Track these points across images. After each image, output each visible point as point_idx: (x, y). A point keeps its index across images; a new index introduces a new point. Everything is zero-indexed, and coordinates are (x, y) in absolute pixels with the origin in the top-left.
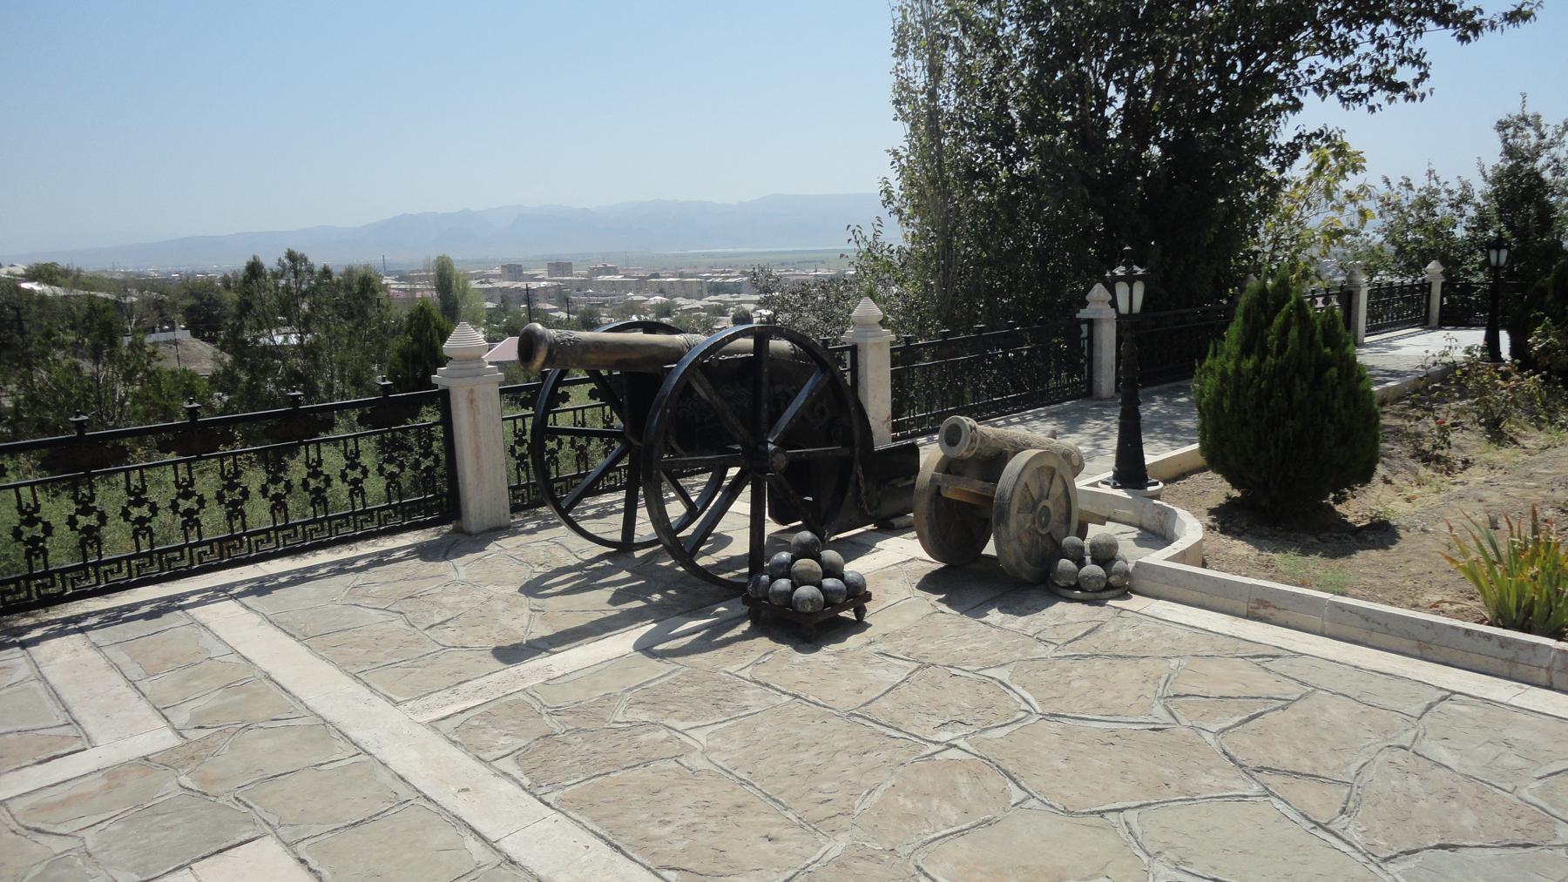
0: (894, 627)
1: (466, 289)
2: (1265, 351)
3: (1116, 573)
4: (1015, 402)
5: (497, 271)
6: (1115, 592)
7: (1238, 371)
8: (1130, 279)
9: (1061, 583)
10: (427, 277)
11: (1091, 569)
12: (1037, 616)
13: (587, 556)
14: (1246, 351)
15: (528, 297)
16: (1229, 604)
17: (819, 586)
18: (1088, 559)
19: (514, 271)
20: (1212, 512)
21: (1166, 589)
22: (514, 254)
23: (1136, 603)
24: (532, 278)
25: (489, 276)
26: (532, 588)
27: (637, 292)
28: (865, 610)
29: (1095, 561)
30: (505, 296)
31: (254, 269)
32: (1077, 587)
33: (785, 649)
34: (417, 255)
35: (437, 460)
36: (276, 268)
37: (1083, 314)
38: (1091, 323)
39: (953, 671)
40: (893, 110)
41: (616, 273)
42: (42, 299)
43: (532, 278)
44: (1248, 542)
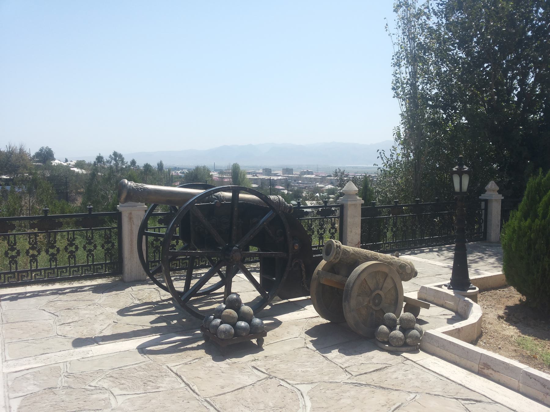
0: (274, 352)
1: (244, 178)
2: (536, 216)
3: (410, 337)
4: (436, 240)
5: (261, 171)
6: (409, 348)
7: (520, 227)
8: (460, 173)
9: (379, 339)
10: (229, 173)
11: (397, 333)
12: (357, 357)
13: (163, 298)
14: (525, 216)
15: (272, 183)
16: (469, 364)
17: (234, 325)
18: (398, 327)
19: (268, 171)
20: (507, 308)
21: (438, 350)
22: (268, 164)
23: (421, 357)
24: (276, 175)
25: (258, 173)
26: (123, 312)
27: (321, 183)
28: (263, 340)
29: (401, 329)
30: (263, 181)
31: (100, 159)
32: (388, 343)
33: (209, 357)
34: (226, 163)
35: (113, 245)
36: (108, 159)
37: (483, 197)
38: (486, 201)
39: (282, 383)
40: (393, 93)
41: (312, 174)
42: (78, 173)
43: (276, 175)
44: (518, 328)
